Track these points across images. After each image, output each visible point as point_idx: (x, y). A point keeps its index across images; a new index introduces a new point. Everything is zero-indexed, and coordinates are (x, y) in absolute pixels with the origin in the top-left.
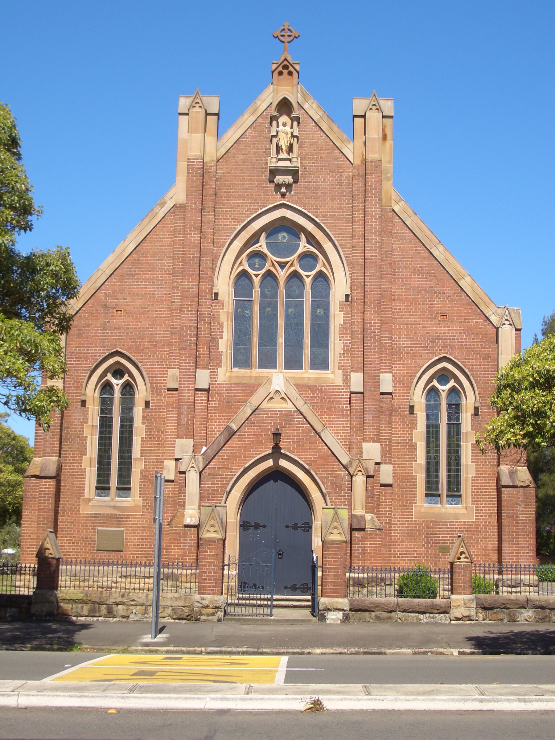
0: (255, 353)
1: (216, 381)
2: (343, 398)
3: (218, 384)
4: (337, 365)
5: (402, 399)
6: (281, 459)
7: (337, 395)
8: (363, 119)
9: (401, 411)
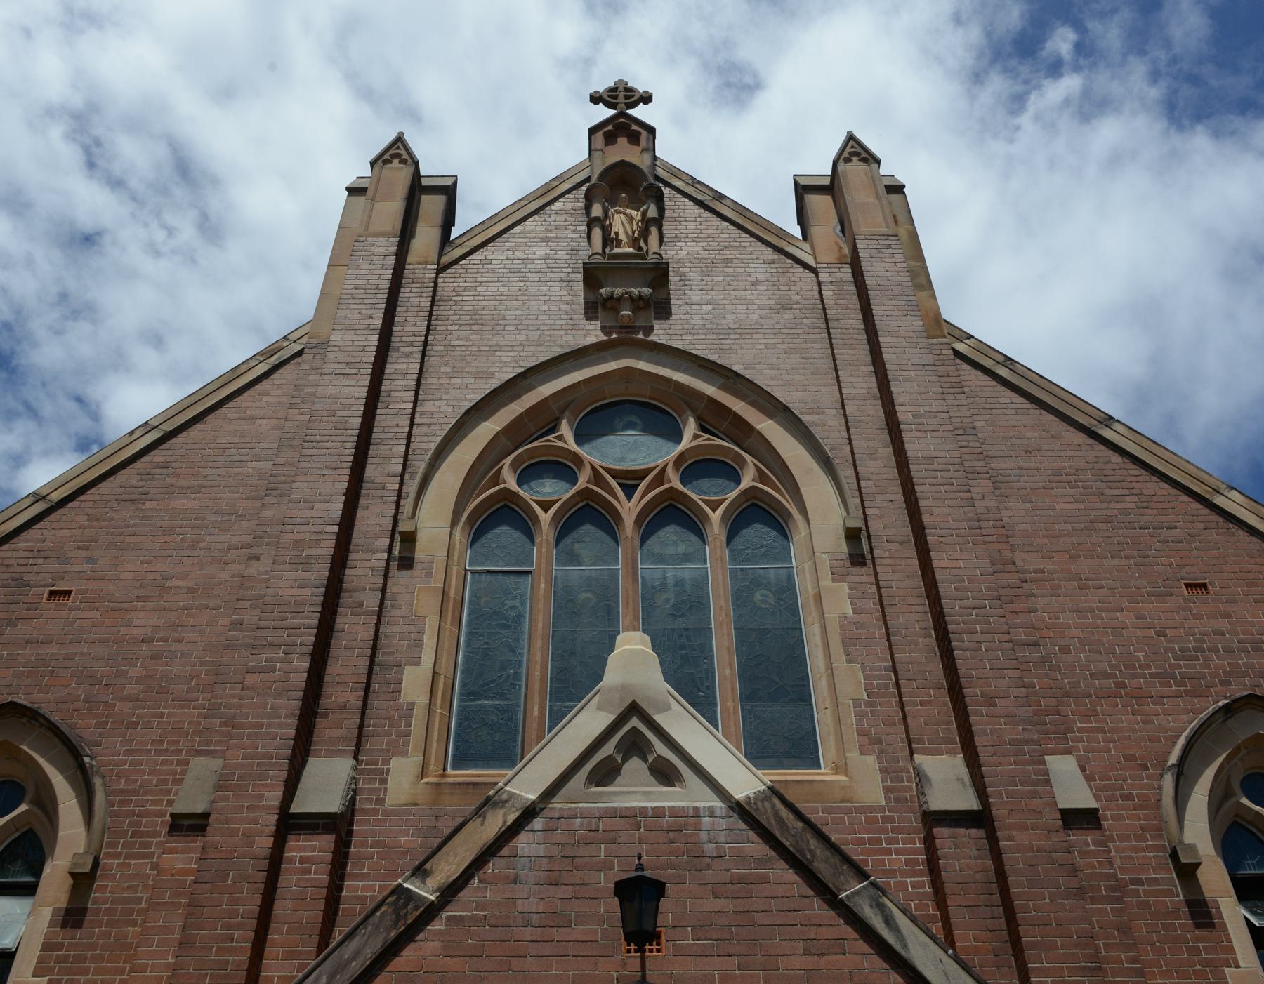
0: (536, 713)
1: (380, 802)
2: (898, 852)
3: (387, 813)
4: (852, 738)
5: (1137, 850)
6: (423, 197)
7: (871, 841)
8: (980, 833)
9: (1146, 893)
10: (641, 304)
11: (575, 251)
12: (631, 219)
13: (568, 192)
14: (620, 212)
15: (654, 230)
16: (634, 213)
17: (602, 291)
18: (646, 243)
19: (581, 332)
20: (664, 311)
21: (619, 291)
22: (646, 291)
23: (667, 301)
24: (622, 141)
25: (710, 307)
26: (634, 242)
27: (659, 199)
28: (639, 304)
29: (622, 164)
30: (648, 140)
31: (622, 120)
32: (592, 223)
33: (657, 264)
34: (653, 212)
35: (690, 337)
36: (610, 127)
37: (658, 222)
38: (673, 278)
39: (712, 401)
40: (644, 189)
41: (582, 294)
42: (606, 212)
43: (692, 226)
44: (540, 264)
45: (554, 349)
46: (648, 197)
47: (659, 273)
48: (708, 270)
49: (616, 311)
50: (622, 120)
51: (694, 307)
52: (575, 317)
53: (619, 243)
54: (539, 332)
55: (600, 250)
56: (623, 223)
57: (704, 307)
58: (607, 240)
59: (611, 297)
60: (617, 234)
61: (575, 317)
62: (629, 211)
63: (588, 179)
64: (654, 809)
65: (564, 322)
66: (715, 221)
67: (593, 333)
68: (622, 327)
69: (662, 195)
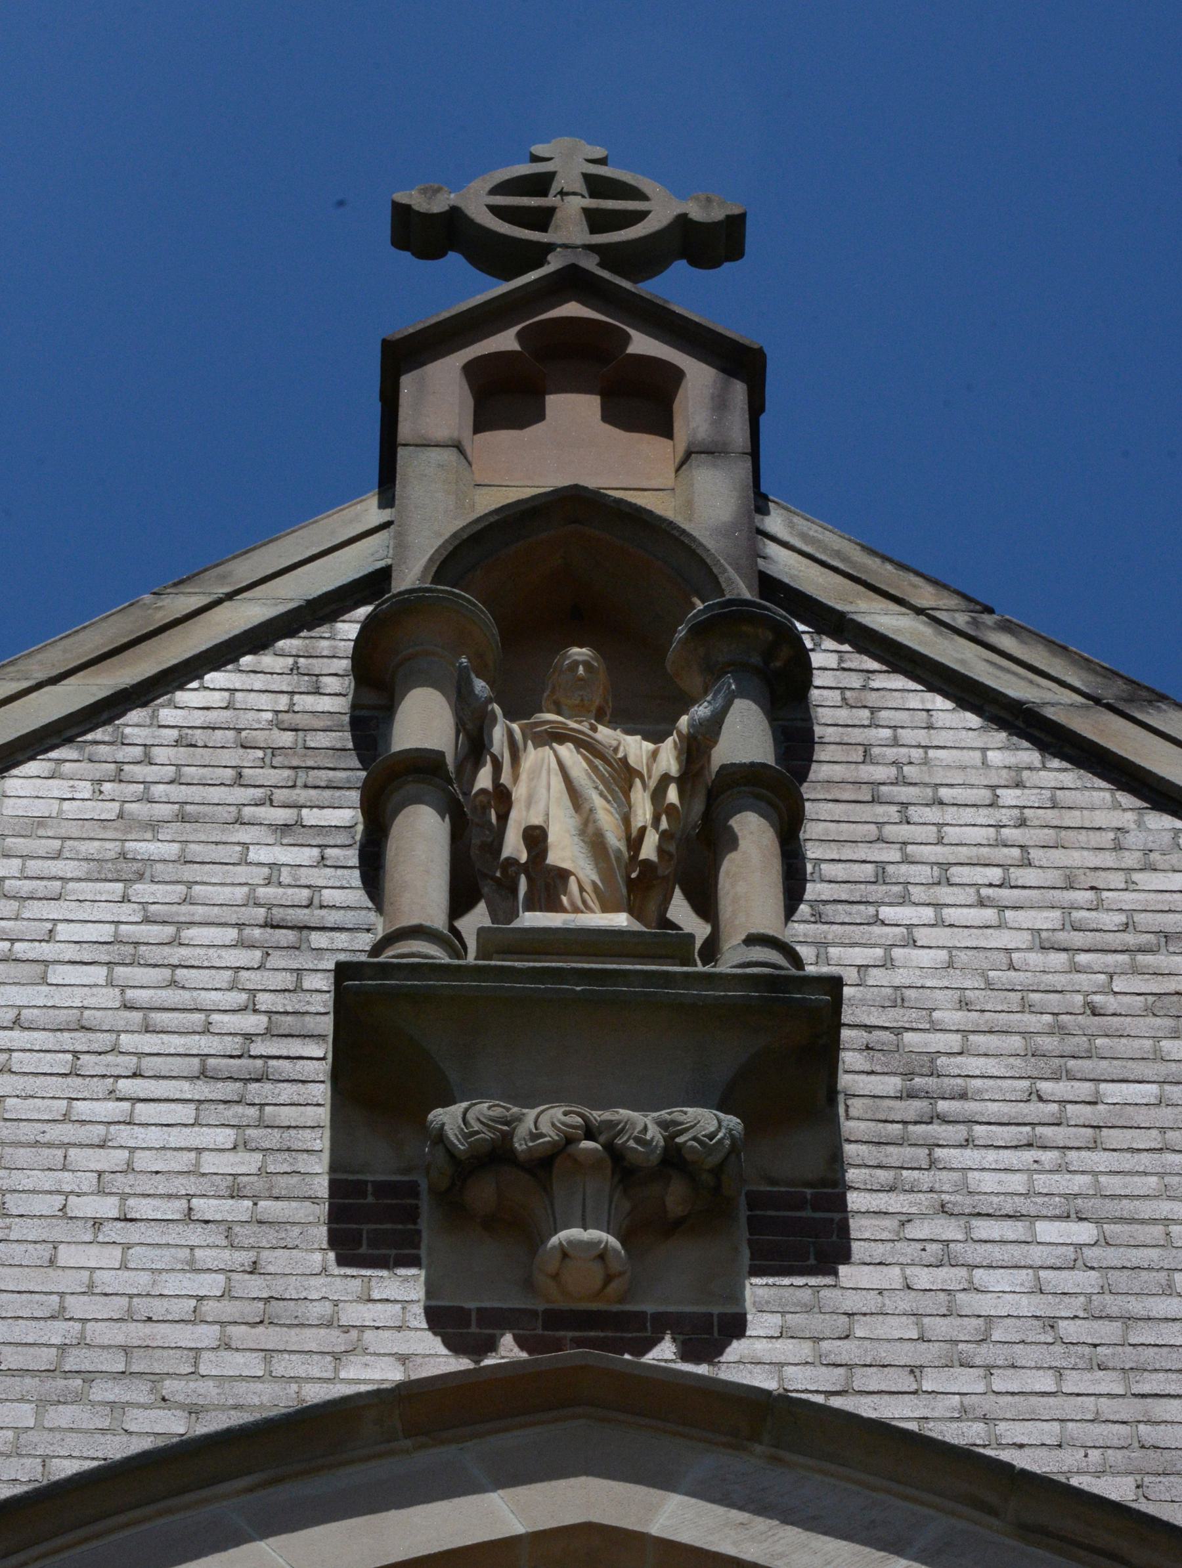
10: (676, 1197)
11: (290, 927)
12: (622, 775)
13: (258, 639)
14: (557, 736)
15: (753, 832)
16: (635, 748)
17: (448, 1118)
18: (705, 903)
19: (311, 1339)
20: (811, 1237)
21: (544, 1121)
22: (705, 1122)
23: (830, 1193)
24: (574, 412)
25: (1084, 1232)
26: (639, 885)
27: (786, 693)
28: (671, 1200)
29: (575, 506)
30: (720, 404)
31: (572, 309)
32: (389, 782)
33: (774, 983)
34: (745, 737)
35: (968, 1381)
36: (506, 341)
37: (780, 790)
38: (859, 1076)
39: (712, 1324)
40: (700, 630)
41: (321, 1141)
42: (475, 745)
43: (970, 830)
44: (82, 987)
45: (139, 1421)
46: (713, 672)
47: (789, 1037)
48: (1067, 1047)
49: (521, 1230)
50: (572, 309)
51: (984, 1229)
52: (275, 1261)
53: (549, 886)
54: (57, 1332)
55: (437, 919)
56: (570, 794)
57: (1047, 1230)
58: (475, 872)
59: (496, 1154)
60: (536, 838)
61: (275, 1261)
62: (605, 734)
63: (373, 584)
64: (722, 1316)
65: (212, 1284)
66: (1100, 803)
67: (382, 1333)
68: (556, 1319)
69: (806, 669)
